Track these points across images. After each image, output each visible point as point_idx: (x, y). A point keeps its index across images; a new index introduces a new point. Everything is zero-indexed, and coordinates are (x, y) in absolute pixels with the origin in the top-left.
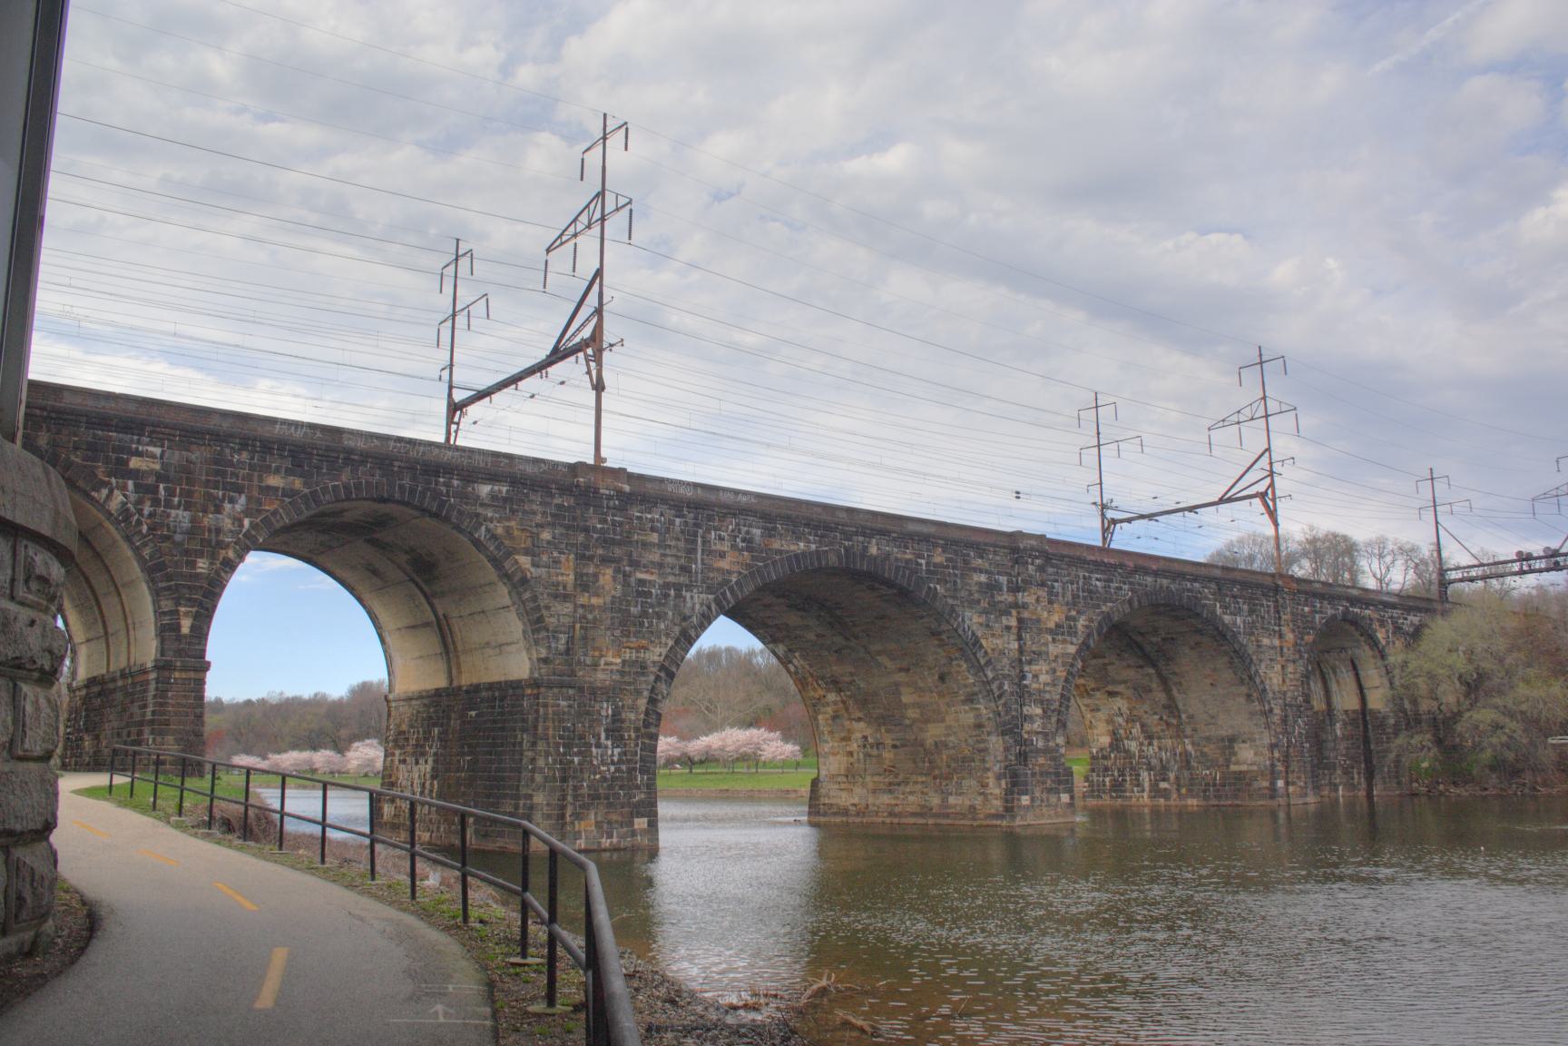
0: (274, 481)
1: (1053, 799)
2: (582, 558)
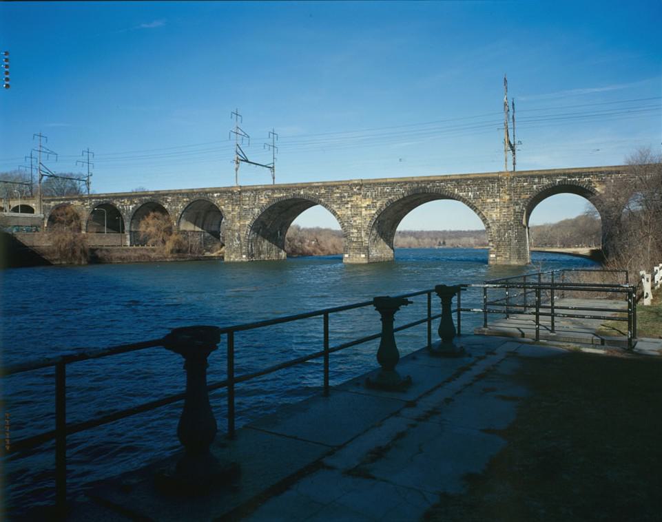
0: (185, 200)
1: (358, 256)
2: (233, 205)
